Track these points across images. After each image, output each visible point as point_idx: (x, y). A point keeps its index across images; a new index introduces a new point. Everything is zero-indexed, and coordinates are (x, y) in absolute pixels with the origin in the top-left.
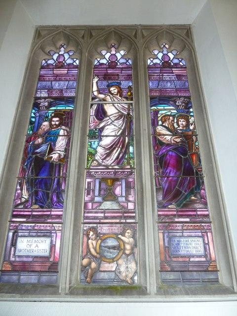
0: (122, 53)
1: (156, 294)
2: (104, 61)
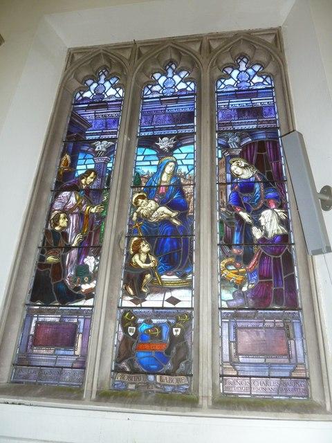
0: (103, 77)
1: (209, 408)
2: (88, 94)
